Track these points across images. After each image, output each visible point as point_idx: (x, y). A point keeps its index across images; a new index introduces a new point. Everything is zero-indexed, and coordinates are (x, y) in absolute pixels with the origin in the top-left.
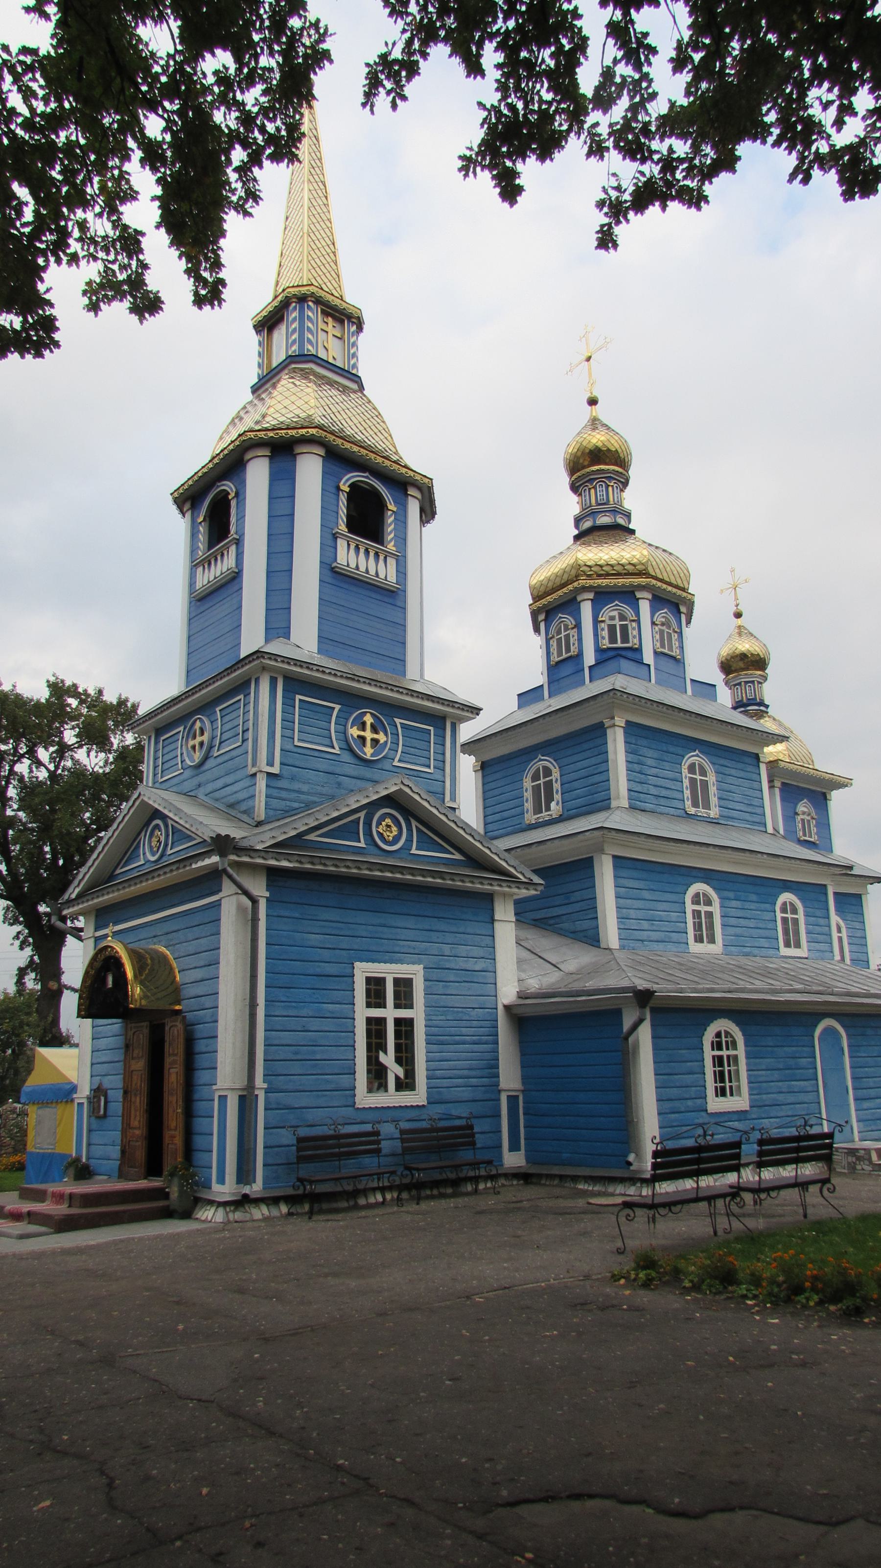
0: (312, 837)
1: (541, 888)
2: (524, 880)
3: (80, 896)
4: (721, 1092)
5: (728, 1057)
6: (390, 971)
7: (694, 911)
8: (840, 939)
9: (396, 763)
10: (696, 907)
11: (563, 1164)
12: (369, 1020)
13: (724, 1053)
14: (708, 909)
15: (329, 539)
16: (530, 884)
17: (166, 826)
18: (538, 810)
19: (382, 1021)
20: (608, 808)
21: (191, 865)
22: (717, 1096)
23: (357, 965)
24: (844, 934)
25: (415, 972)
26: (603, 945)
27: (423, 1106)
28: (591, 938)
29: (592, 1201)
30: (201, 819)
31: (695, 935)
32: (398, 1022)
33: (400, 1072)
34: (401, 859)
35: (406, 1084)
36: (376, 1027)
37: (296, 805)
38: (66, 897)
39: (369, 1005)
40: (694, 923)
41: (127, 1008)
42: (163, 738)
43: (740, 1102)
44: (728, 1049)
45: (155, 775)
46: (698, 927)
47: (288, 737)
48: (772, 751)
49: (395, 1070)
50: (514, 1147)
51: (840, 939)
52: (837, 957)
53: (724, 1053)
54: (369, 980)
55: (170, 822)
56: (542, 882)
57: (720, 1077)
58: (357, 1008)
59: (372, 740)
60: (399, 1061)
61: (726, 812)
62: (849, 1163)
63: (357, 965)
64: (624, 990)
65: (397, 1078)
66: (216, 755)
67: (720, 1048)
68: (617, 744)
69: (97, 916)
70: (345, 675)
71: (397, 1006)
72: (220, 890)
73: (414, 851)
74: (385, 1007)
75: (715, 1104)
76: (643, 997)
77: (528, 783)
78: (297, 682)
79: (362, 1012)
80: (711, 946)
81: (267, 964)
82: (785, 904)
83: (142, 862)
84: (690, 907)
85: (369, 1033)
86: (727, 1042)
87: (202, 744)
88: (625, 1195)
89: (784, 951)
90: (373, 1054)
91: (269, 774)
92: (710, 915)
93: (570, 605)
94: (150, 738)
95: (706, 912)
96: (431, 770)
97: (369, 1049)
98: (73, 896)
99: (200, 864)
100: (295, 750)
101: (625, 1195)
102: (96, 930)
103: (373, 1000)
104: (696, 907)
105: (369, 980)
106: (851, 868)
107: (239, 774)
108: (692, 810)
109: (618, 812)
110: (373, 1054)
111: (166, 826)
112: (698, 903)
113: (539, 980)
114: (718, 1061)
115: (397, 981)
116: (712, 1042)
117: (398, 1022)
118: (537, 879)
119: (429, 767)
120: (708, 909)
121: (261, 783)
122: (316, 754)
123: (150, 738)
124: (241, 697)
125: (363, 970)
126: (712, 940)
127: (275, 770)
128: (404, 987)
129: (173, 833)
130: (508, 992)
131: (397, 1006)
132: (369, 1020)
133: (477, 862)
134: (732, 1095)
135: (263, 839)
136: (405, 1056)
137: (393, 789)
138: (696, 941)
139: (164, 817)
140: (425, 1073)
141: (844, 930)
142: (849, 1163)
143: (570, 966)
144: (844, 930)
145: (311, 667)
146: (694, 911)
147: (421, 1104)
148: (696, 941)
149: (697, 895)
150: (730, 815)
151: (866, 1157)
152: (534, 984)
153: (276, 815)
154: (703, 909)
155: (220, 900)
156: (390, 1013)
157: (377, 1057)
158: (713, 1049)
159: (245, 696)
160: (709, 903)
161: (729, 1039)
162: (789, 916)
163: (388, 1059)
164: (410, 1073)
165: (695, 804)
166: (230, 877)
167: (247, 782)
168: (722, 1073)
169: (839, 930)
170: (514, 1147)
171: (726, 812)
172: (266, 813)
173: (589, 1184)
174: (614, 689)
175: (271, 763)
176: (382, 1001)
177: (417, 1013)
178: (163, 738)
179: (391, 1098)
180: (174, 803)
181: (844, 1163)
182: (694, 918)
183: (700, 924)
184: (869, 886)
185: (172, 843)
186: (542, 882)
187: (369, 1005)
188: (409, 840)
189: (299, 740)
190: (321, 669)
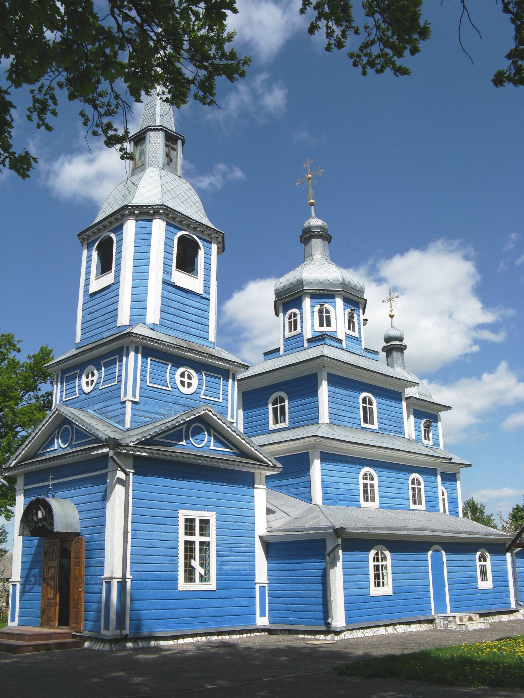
0: (157, 439)
1: (281, 470)
2: (272, 465)
3: (15, 467)
4: (377, 585)
5: (382, 566)
6: (198, 515)
7: (364, 483)
8: (444, 499)
9: (201, 396)
10: (365, 481)
11: (291, 623)
12: (186, 542)
13: (380, 563)
14: (372, 482)
15: (167, 272)
16: (275, 466)
17: (72, 428)
18: (276, 422)
19: (192, 543)
20: (317, 423)
21: (90, 452)
22: (375, 586)
23: (180, 511)
24: (446, 497)
25: (212, 516)
26: (313, 502)
27: (214, 591)
28: (309, 499)
29: (309, 642)
30: (96, 427)
31: (364, 497)
32: (202, 543)
33: (202, 571)
34: (204, 452)
35: (204, 578)
36: (189, 546)
37: (147, 420)
38: (7, 465)
39: (186, 534)
40: (364, 490)
41: (52, 531)
42: (66, 376)
43: (387, 590)
44: (382, 561)
45: (61, 396)
46: (366, 492)
47: (143, 380)
48: (409, 392)
49: (199, 570)
50: (263, 615)
51: (444, 499)
52: (442, 510)
53: (380, 563)
54: (186, 520)
55: (75, 426)
56: (282, 466)
57: (377, 577)
58: (179, 535)
59: (184, 378)
60: (202, 565)
61: (382, 426)
62: (444, 624)
63: (180, 511)
64: (329, 528)
65: (201, 575)
66: (101, 388)
67: (377, 560)
68: (324, 389)
69: (25, 478)
70: (176, 346)
71: (201, 535)
72: (107, 467)
73: (212, 447)
74: (195, 535)
75: (374, 591)
76: (338, 532)
77: (270, 408)
78: (152, 351)
79: (182, 538)
80: (373, 503)
81: (132, 509)
82: (414, 479)
83: (56, 447)
84: (361, 481)
85: (186, 549)
86: (382, 557)
87: (92, 381)
88: (325, 640)
89: (413, 506)
90: (188, 561)
91: (134, 402)
92: (372, 486)
93: (297, 303)
94: (58, 375)
95: (370, 484)
96: (221, 400)
97: (186, 558)
98: (12, 465)
99: (95, 452)
100: (148, 388)
101: (325, 640)
102: (25, 485)
103: (188, 531)
104: (365, 481)
105: (186, 520)
106: (451, 459)
107: (116, 401)
108: (363, 425)
109: (323, 426)
110: (188, 561)
111: (72, 428)
112: (366, 479)
113: (280, 521)
114: (376, 568)
115: (201, 521)
116: (374, 557)
117: (202, 543)
118: (279, 465)
119: (219, 398)
120: (372, 482)
121: (129, 405)
122: (162, 391)
123: (58, 375)
124: (117, 356)
125: (183, 514)
126: (373, 500)
127: (137, 400)
128: (205, 523)
129: (76, 433)
130: (261, 528)
131: (201, 535)
132: (186, 542)
133: (244, 454)
134: (383, 586)
135: (131, 440)
136: (205, 563)
137: (203, 412)
138: (364, 501)
139: (71, 423)
140: (215, 572)
141: (446, 494)
142: (444, 624)
143: (294, 513)
144: (446, 494)
145: (158, 341)
146: (364, 483)
147: (213, 589)
148: (364, 501)
149: (366, 474)
150: (385, 428)
151: (453, 620)
152: (276, 525)
153: (137, 425)
154: (369, 482)
155: (107, 473)
156: (197, 538)
157: (190, 563)
158: (374, 561)
159: (119, 356)
160: (372, 479)
161: (383, 556)
162: (416, 486)
163: (195, 563)
164: (207, 572)
165: (366, 421)
166: (114, 461)
167: (119, 406)
168: (378, 574)
169: (443, 495)
170: (263, 615)
171: (382, 426)
172: (131, 424)
173: (305, 635)
174: (323, 356)
175: (134, 396)
176: (193, 532)
177: (212, 539)
178: (66, 376)
179: (197, 586)
180: (78, 416)
181: (442, 624)
182: (364, 488)
183: (367, 491)
184: (461, 469)
185: (76, 438)
186: (282, 466)
187: (186, 534)
188: (209, 441)
189: (150, 382)
190: (163, 343)
